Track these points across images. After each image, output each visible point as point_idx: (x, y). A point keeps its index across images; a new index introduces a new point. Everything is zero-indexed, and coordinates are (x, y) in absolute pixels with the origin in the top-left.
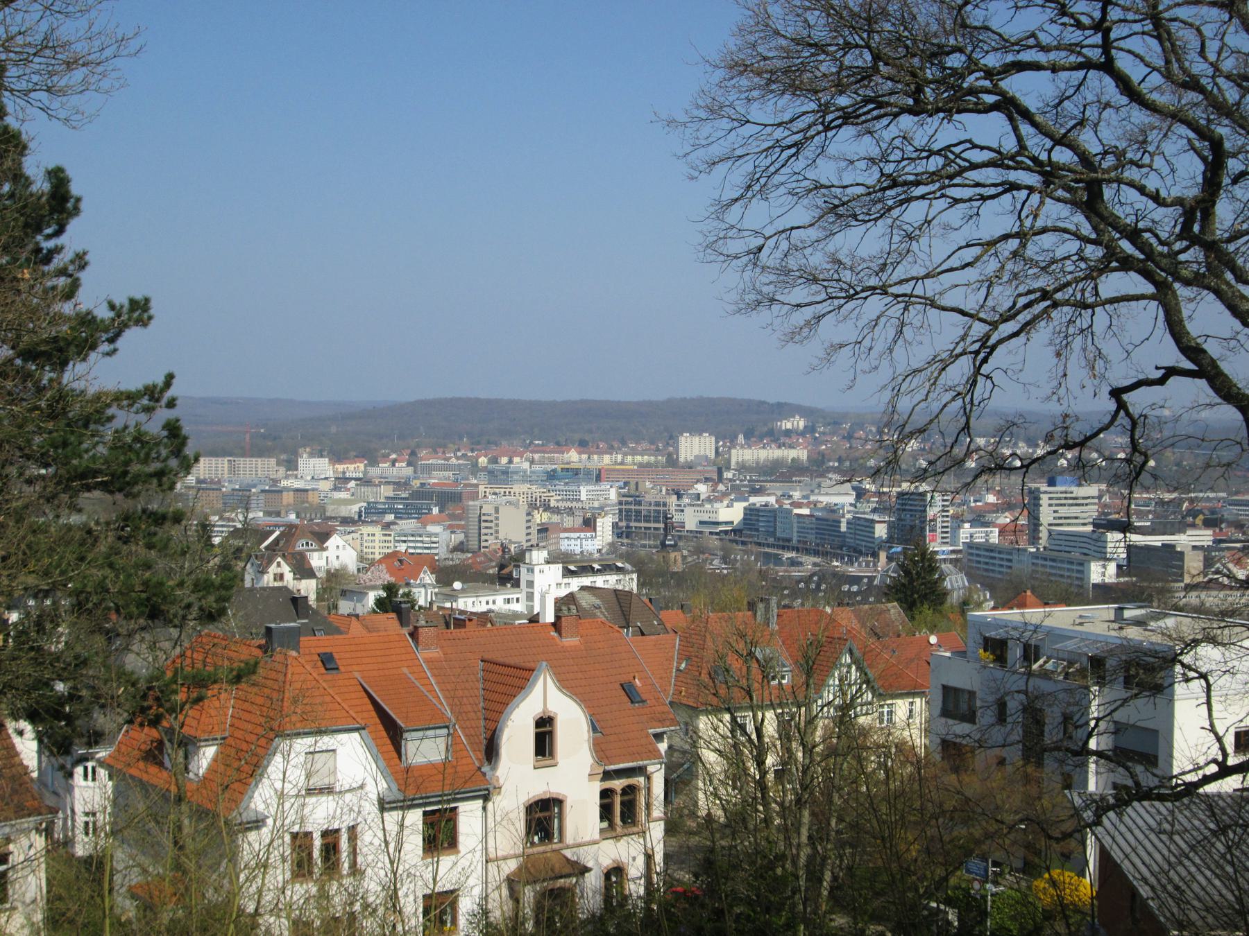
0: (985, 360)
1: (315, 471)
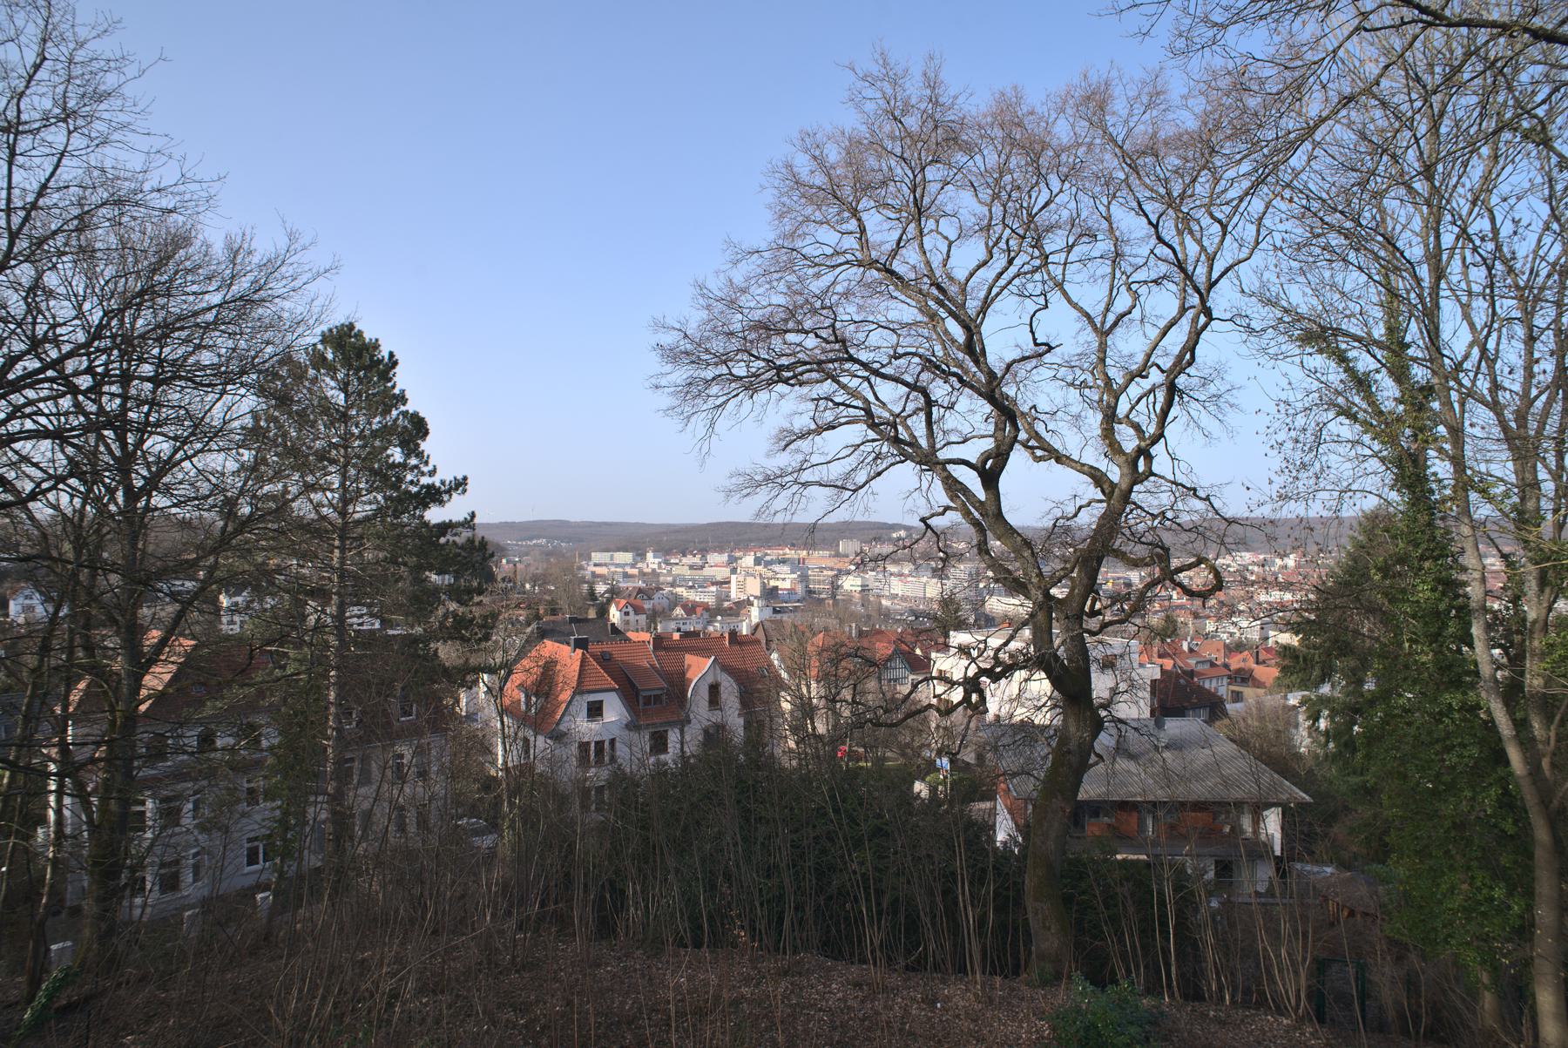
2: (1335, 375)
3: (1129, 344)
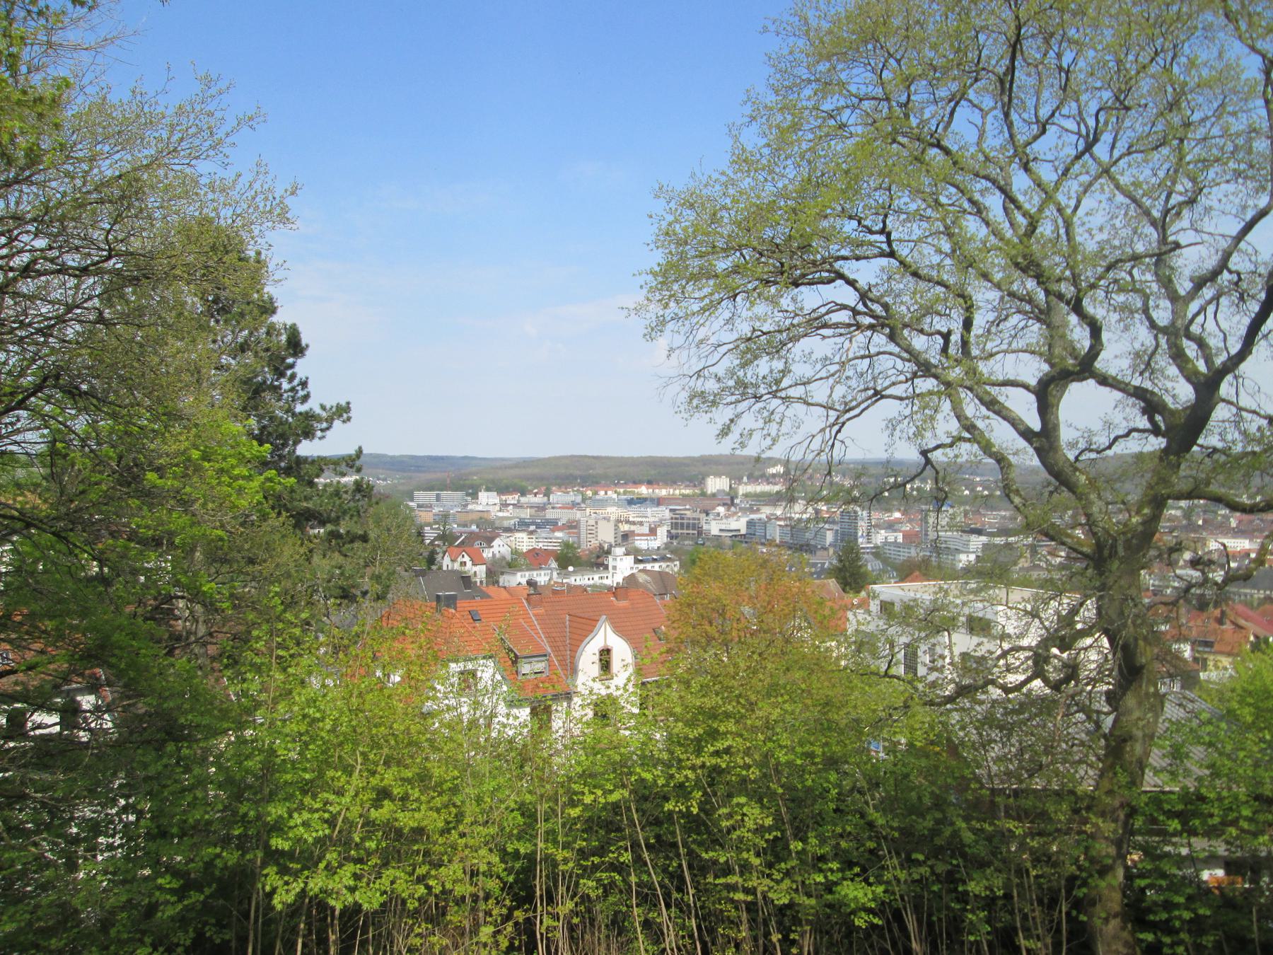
0: (839, 431)
1: (487, 501)
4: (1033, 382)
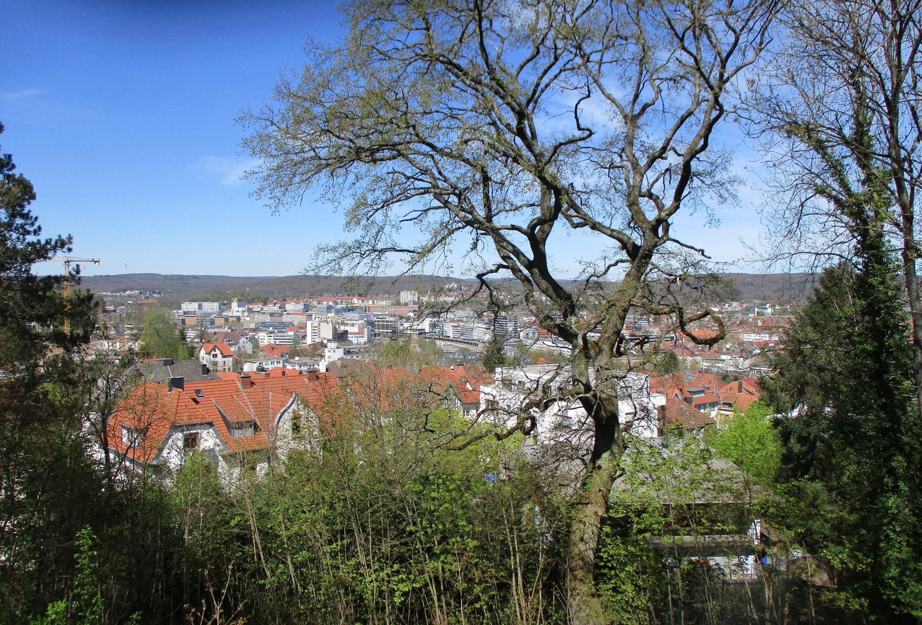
2: (817, 162)
3: (652, 135)
4: (525, 226)
